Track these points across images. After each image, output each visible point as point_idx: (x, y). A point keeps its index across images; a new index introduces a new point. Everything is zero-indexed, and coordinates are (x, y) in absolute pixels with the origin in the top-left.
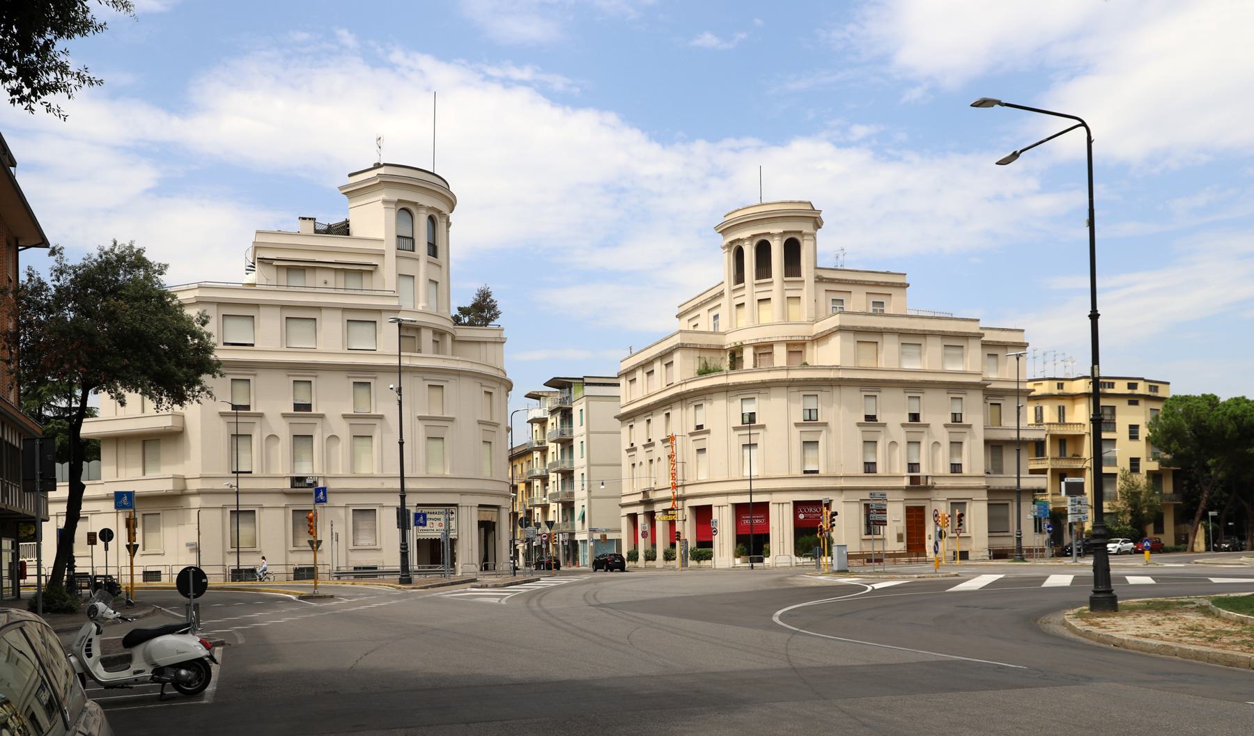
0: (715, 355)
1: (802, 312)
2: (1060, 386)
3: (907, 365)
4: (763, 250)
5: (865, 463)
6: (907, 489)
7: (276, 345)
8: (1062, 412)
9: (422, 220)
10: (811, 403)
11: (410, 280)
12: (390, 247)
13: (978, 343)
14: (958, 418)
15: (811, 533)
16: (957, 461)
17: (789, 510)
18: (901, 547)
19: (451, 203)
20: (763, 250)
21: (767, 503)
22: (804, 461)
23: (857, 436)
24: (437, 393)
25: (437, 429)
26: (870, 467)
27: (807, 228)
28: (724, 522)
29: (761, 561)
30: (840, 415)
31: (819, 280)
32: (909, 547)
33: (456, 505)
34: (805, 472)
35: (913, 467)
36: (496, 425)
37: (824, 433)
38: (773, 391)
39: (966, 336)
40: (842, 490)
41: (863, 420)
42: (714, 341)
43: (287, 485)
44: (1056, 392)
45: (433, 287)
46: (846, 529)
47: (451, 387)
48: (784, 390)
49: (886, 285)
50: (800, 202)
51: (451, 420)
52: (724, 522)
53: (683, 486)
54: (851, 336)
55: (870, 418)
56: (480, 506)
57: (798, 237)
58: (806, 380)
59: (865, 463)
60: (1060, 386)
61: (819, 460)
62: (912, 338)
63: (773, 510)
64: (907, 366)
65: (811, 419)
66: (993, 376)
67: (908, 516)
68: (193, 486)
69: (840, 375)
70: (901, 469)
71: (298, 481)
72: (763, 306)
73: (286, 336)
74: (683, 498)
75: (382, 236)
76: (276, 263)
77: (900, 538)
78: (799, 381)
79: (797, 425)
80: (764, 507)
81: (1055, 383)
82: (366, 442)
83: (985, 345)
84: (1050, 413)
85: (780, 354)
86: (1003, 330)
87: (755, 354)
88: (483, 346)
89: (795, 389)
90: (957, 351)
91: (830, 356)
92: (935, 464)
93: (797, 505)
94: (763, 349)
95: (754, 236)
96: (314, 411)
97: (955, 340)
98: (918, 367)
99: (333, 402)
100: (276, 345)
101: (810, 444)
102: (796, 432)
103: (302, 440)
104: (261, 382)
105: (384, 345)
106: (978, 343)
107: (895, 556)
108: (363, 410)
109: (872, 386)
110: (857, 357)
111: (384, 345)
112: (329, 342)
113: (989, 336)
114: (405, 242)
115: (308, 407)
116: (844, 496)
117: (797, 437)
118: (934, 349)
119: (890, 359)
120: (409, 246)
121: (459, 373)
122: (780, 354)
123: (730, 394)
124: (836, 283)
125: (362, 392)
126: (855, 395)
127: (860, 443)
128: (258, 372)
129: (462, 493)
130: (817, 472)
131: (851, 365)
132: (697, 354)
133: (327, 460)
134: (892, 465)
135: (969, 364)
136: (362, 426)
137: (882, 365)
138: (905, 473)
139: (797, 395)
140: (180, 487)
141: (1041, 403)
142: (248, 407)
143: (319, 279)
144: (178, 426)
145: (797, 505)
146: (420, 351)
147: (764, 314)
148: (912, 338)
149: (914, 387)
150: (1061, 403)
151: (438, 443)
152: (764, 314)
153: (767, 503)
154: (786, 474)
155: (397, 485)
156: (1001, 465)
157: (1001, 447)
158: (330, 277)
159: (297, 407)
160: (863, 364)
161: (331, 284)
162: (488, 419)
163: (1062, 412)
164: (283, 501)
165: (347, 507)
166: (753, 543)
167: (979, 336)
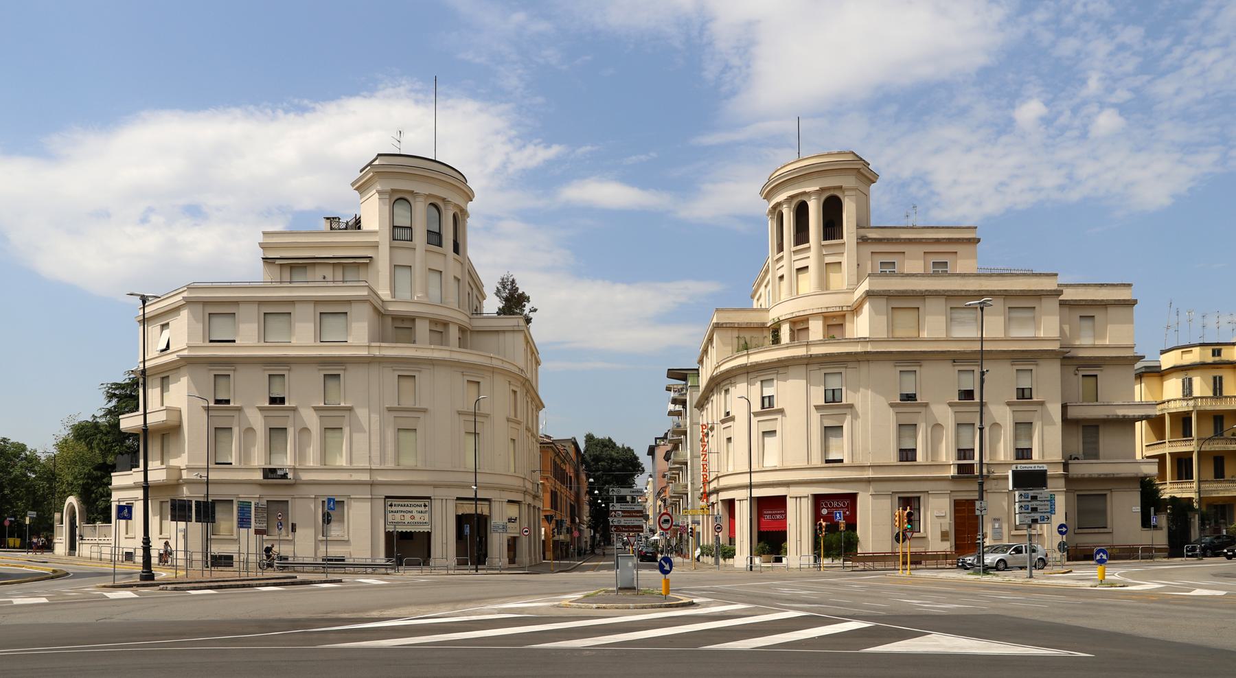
0: (756, 334)
1: (840, 280)
2: (1216, 353)
3: (1016, 333)
4: (801, 212)
5: (901, 450)
7: (311, 342)
8: (1218, 385)
10: (834, 383)
11: (407, 271)
12: (384, 239)
13: (1053, 304)
14: (1027, 394)
15: (836, 534)
16: (908, 445)
17: (807, 507)
18: (947, 546)
20: (801, 212)
22: (825, 449)
23: (890, 419)
24: (474, 388)
25: (405, 420)
26: (907, 455)
27: (848, 181)
28: (799, 523)
29: (779, 560)
31: (863, 240)
32: (957, 547)
33: (429, 498)
34: (828, 461)
35: (964, 453)
36: (519, 423)
37: (849, 417)
38: (792, 371)
39: (1038, 295)
40: (869, 481)
42: (754, 318)
43: (259, 476)
44: (1210, 359)
45: (435, 278)
46: (874, 524)
47: (424, 378)
48: (803, 369)
49: (955, 241)
50: (839, 153)
51: (425, 411)
52: (799, 523)
53: (718, 478)
54: (882, 303)
55: (910, 397)
56: (458, 499)
58: (825, 355)
59: (901, 450)
60: (1216, 353)
61: (841, 449)
62: (979, 301)
63: (790, 503)
65: (833, 398)
66: (1086, 341)
67: (956, 511)
68: (185, 475)
69: (869, 348)
70: (947, 455)
71: (269, 473)
73: (264, 334)
74: (717, 491)
75: (377, 228)
76: (278, 262)
77: (944, 536)
78: (817, 356)
79: (817, 408)
80: (780, 502)
81: (1209, 351)
82: (337, 434)
83: (1063, 304)
84: (1201, 386)
85: (816, 329)
86: (1102, 285)
87: (791, 330)
88: (501, 337)
89: (816, 367)
90: (1028, 314)
93: (818, 500)
94: (799, 325)
95: (792, 197)
97: (1023, 302)
99: (304, 393)
100: (311, 342)
101: (831, 431)
102: (815, 416)
103: (276, 433)
104: (353, 379)
105: (357, 337)
106: (1053, 304)
107: (935, 557)
108: (407, 402)
109: (911, 360)
110: (891, 326)
111: (357, 337)
112: (301, 339)
113: (1068, 295)
114: (400, 234)
115: (282, 400)
119: (934, 328)
120: (437, 241)
121: (432, 362)
122: (816, 329)
123: (750, 376)
124: (883, 244)
125: (406, 384)
126: (889, 372)
128: (293, 367)
129: (436, 486)
130: (841, 461)
132: (736, 334)
133: (300, 453)
135: (1047, 328)
136: (335, 421)
137: (925, 334)
138: (952, 459)
139: (818, 374)
140: (174, 476)
141: (1190, 374)
142: (228, 402)
143: (319, 273)
144: (173, 421)
145: (818, 500)
146: (414, 342)
148: (979, 301)
150: (1217, 373)
151: (410, 435)
154: (804, 464)
156: (1097, 449)
157: (1097, 427)
158: (328, 273)
160: (899, 333)
161: (330, 277)
162: (396, 405)
163: (1218, 385)
166: (771, 542)
167: (1057, 293)
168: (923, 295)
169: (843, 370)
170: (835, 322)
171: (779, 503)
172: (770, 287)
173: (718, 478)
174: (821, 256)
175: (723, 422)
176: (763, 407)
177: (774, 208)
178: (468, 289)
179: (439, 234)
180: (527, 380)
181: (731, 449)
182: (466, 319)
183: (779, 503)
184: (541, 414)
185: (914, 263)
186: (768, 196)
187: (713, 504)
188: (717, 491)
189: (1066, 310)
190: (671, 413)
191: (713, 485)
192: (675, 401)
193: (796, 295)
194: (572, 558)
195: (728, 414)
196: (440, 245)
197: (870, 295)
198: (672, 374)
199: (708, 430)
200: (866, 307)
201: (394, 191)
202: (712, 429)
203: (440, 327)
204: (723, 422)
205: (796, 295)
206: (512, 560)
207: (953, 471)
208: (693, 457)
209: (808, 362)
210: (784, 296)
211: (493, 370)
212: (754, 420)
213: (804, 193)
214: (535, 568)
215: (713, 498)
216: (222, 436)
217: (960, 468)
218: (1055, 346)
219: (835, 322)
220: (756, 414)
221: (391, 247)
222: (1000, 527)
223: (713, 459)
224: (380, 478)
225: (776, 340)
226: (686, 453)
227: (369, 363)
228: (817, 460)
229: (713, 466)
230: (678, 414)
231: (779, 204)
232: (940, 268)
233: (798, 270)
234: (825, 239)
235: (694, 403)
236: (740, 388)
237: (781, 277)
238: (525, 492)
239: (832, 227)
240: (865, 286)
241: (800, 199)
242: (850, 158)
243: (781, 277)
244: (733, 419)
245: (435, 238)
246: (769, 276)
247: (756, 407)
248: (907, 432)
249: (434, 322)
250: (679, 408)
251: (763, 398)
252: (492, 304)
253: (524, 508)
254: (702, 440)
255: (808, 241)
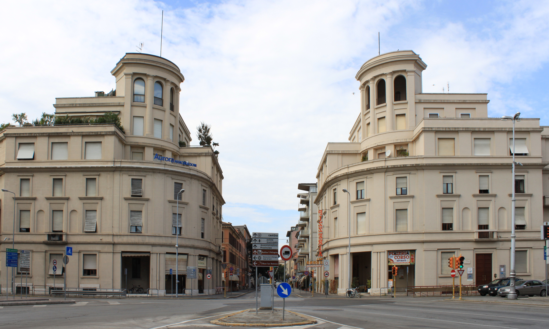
4: (381, 85)
5: (443, 224)
6: (476, 242)
7: (79, 159)
9: (168, 88)
12: (128, 102)
17: (384, 257)
19: (181, 79)
20: (381, 85)
21: (370, 253)
23: (437, 205)
27: (410, 67)
30: (425, 188)
36: (207, 209)
41: (478, 193)
43: (46, 238)
53: (328, 242)
54: (432, 135)
57: (404, 74)
59: (443, 224)
64: (478, 154)
72: (381, 122)
74: (327, 250)
75: (124, 95)
79: (391, 198)
91: (420, 151)
92: (502, 221)
94: (380, 150)
96: (408, 194)
98: (488, 154)
101: (400, 212)
110: (438, 149)
115: (486, 191)
116: (426, 246)
117: (391, 206)
118: (464, 140)
119: (463, 149)
120: (160, 103)
122: (390, 151)
124: (436, 103)
127: (439, 210)
131: (433, 155)
134: (467, 224)
137: (458, 154)
138: (476, 229)
147: (395, 125)
149: (484, 168)
152: (395, 125)
153: (370, 253)
154: (383, 233)
155: (352, 235)
159: (481, 191)
160: (443, 153)
164: (44, 248)
165: (79, 252)
168: (456, 131)
169: (407, 175)
170: (401, 150)
171: (367, 256)
172: (361, 130)
173: (328, 242)
174: (393, 110)
175: (332, 208)
176: (357, 199)
177: (364, 84)
178: (179, 132)
179: (162, 100)
180: (214, 185)
181: (337, 225)
182: (177, 149)
183: (367, 256)
184: (223, 207)
185: (449, 111)
186: (359, 78)
187: (325, 258)
188: (327, 250)
189: (544, 141)
190: (300, 210)
191: (325, 247)
192: (302, 202)
193: (377, 133)
194: (237, 291)
195: (335, 203)
196: (162, 106)
197: (425, 130)
198: (302, 187)
199: (323, 214)
200: (422, 138)
201: (134, 74)
202: (325, 213)
203: (159, 152)
204: (332, 208)
205: (377, 133)
206: (201, 290)
207: (476, 237)
208: (312, 233)
209: (386, 170)
210: (370, 135)
211: (192, 177)
212: (352, 206)
213: (383, 75)
214: (218, 295)
215: (325, 255)
216: (24, 214)
217: (481, 235)
218: (539, 161)
219: (401, 150)
220: (353, 202)
221: (132, 106)
222: (505, 271)
223: (325, 230)
224: (116, 240)
225: (365, 158)
226: (308, 231)
227: (114, 171)
228: (391, 230)
229: (325, 236)
230: (304, 210)
231: (367, 82)
232: (465, 116)
233: (379, 119)
234: (395, 100)
235: (314, 200)
236: (343, 185)
237: (369, 124)
238: (210, 250)
239: (400, 92)
240: (422, 126)
241: (380, 78)
242: (411, 53)
243: (369, 124)
244: (338, 206)
245: (158, 101)
246: (361, 124)
247: (354, 198)
248: (447, 212)
249: (156, 149)
250: (304, 206)
251: (357, 191)
252: (195, 142)
253: (210, 260)
254: (319, 222)
255: (385, 102)
